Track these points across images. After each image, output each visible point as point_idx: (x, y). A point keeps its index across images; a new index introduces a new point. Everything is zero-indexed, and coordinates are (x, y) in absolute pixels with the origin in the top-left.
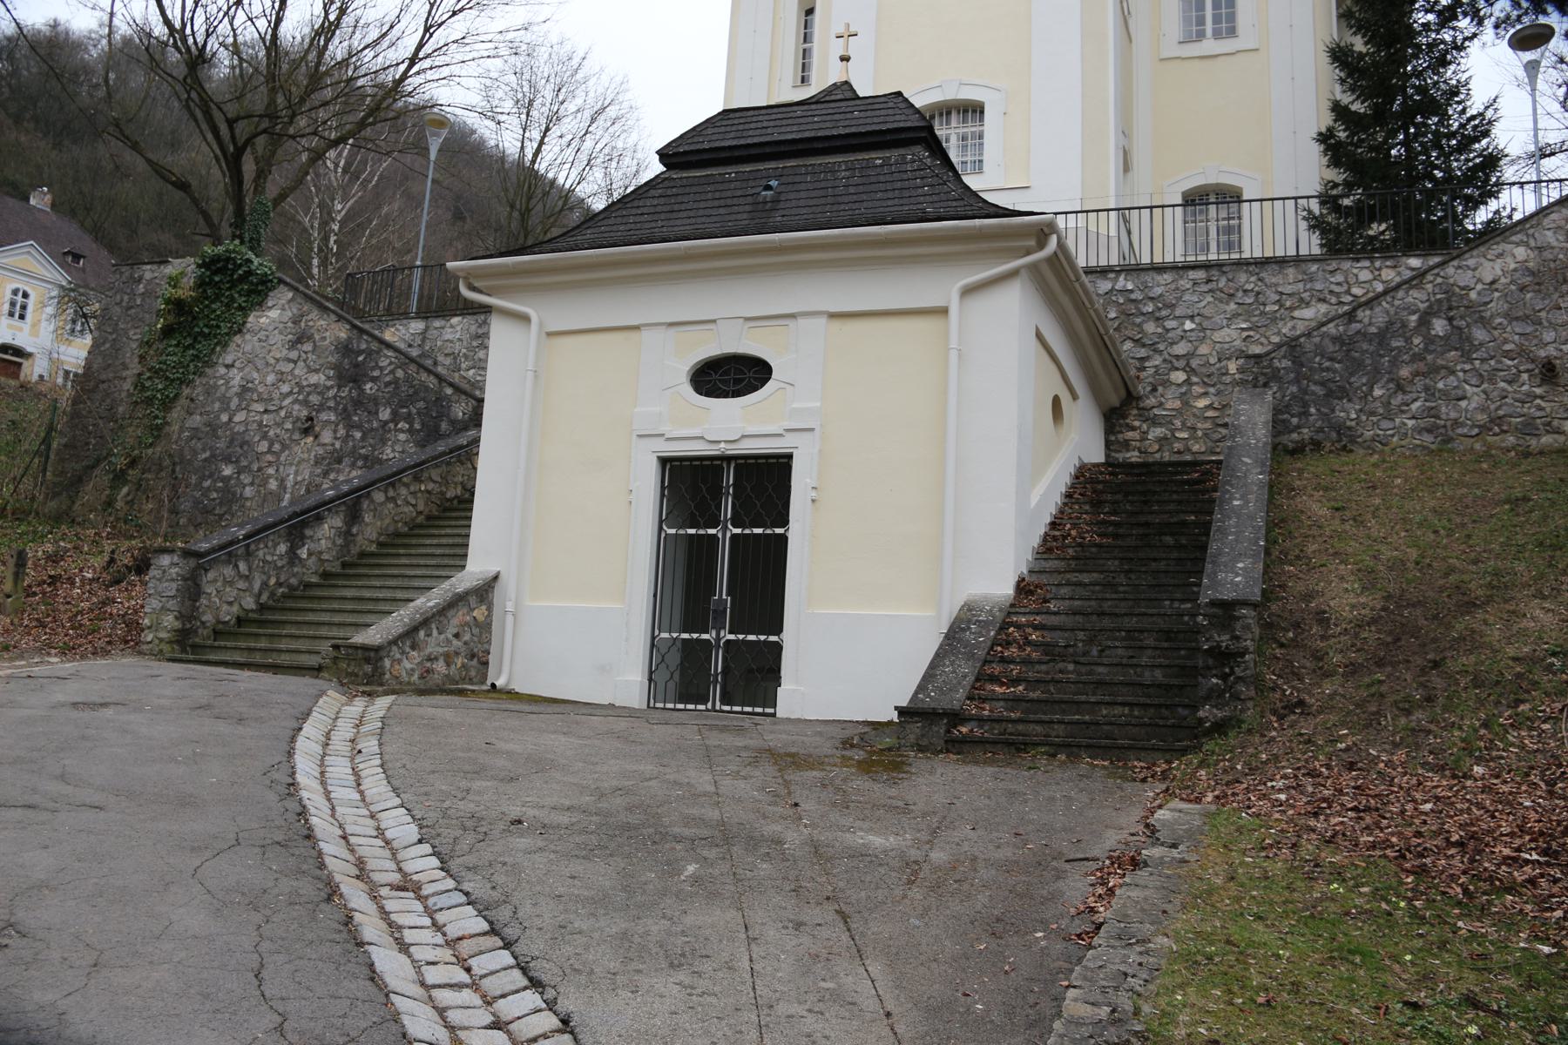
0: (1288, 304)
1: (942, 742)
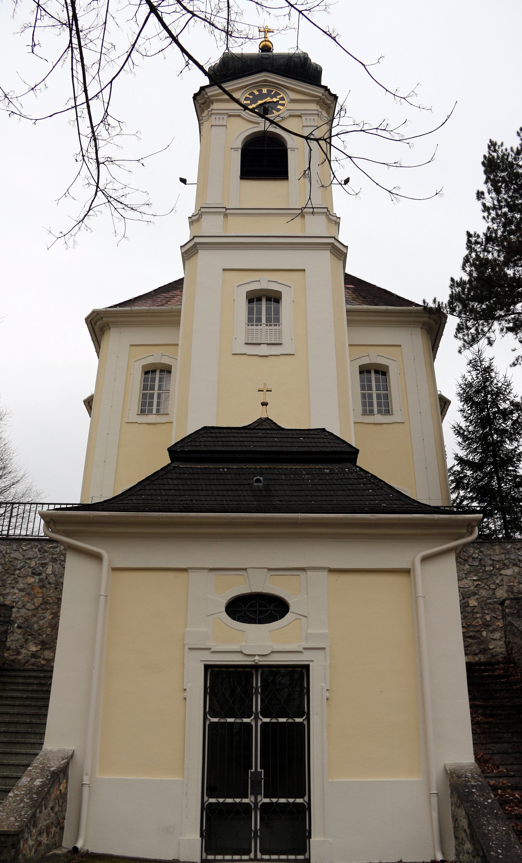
0: (498, 566)
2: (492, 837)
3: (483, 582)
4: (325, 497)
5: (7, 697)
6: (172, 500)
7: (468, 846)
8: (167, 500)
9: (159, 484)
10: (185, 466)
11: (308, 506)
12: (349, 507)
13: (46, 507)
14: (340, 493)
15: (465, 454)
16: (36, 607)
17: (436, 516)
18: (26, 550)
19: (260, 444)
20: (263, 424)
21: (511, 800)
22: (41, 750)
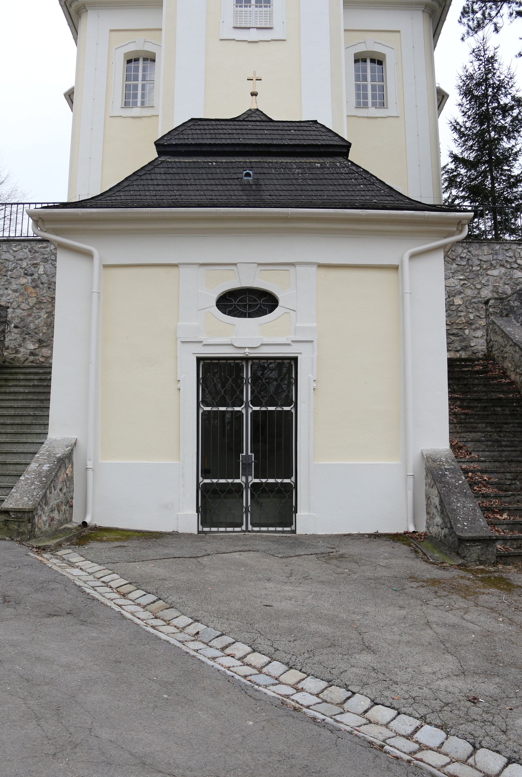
0: (485, 267)
1: (494, 557)
2: (460, 512)
3: (469, 282)
4: (316, 192)
5: (10, 393)
6: (160, 196)
7: (438, 520)
8: (156, 195)
9: (147, 179)
10: (173, 160)
11: (298, 201)
12: (339, 202)
13: (33, 206)
14: (330, 188)
15: (461, 151)
16: (31, 307)
17: (427, 213)
18: (16, 251)
19: (250, 136)
20: (252, 115)
21: (480, 482)
22: (46, 439)
